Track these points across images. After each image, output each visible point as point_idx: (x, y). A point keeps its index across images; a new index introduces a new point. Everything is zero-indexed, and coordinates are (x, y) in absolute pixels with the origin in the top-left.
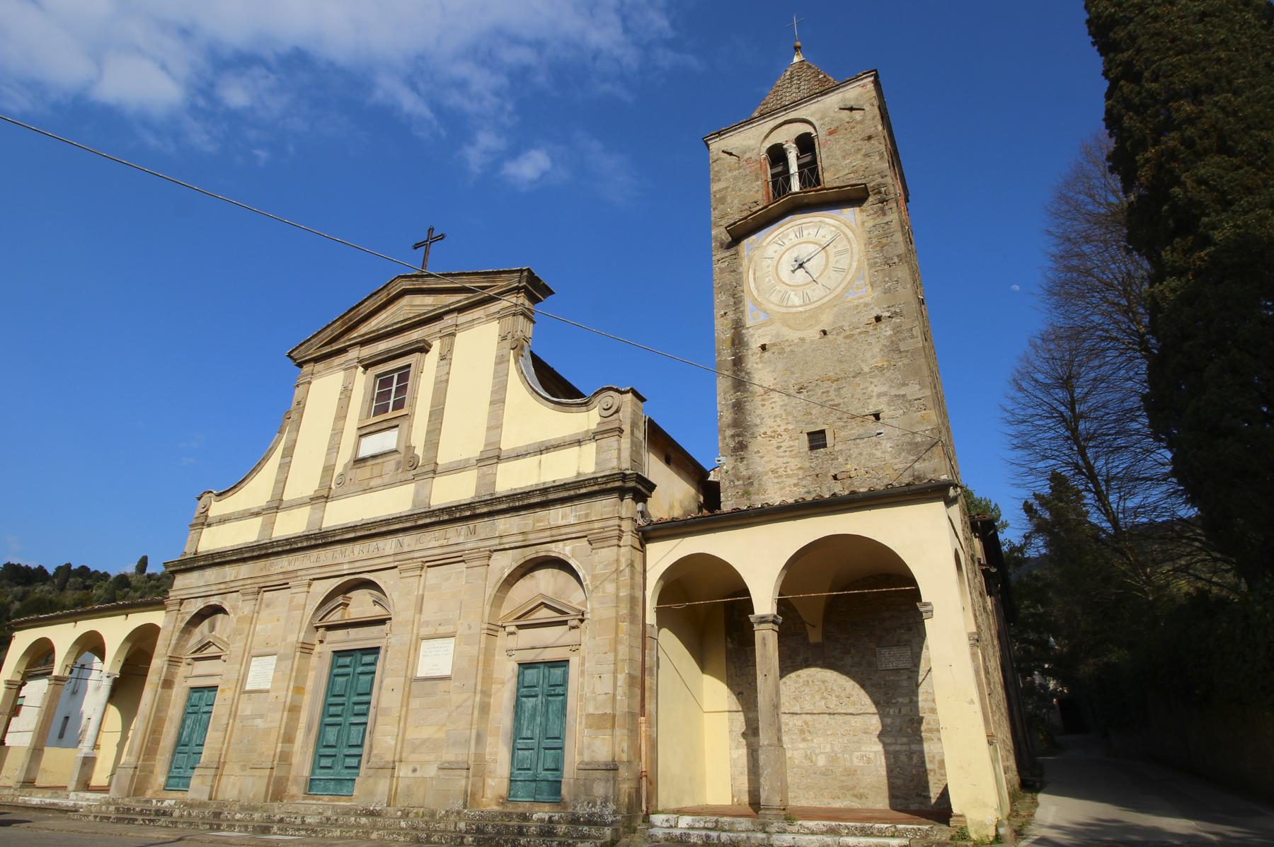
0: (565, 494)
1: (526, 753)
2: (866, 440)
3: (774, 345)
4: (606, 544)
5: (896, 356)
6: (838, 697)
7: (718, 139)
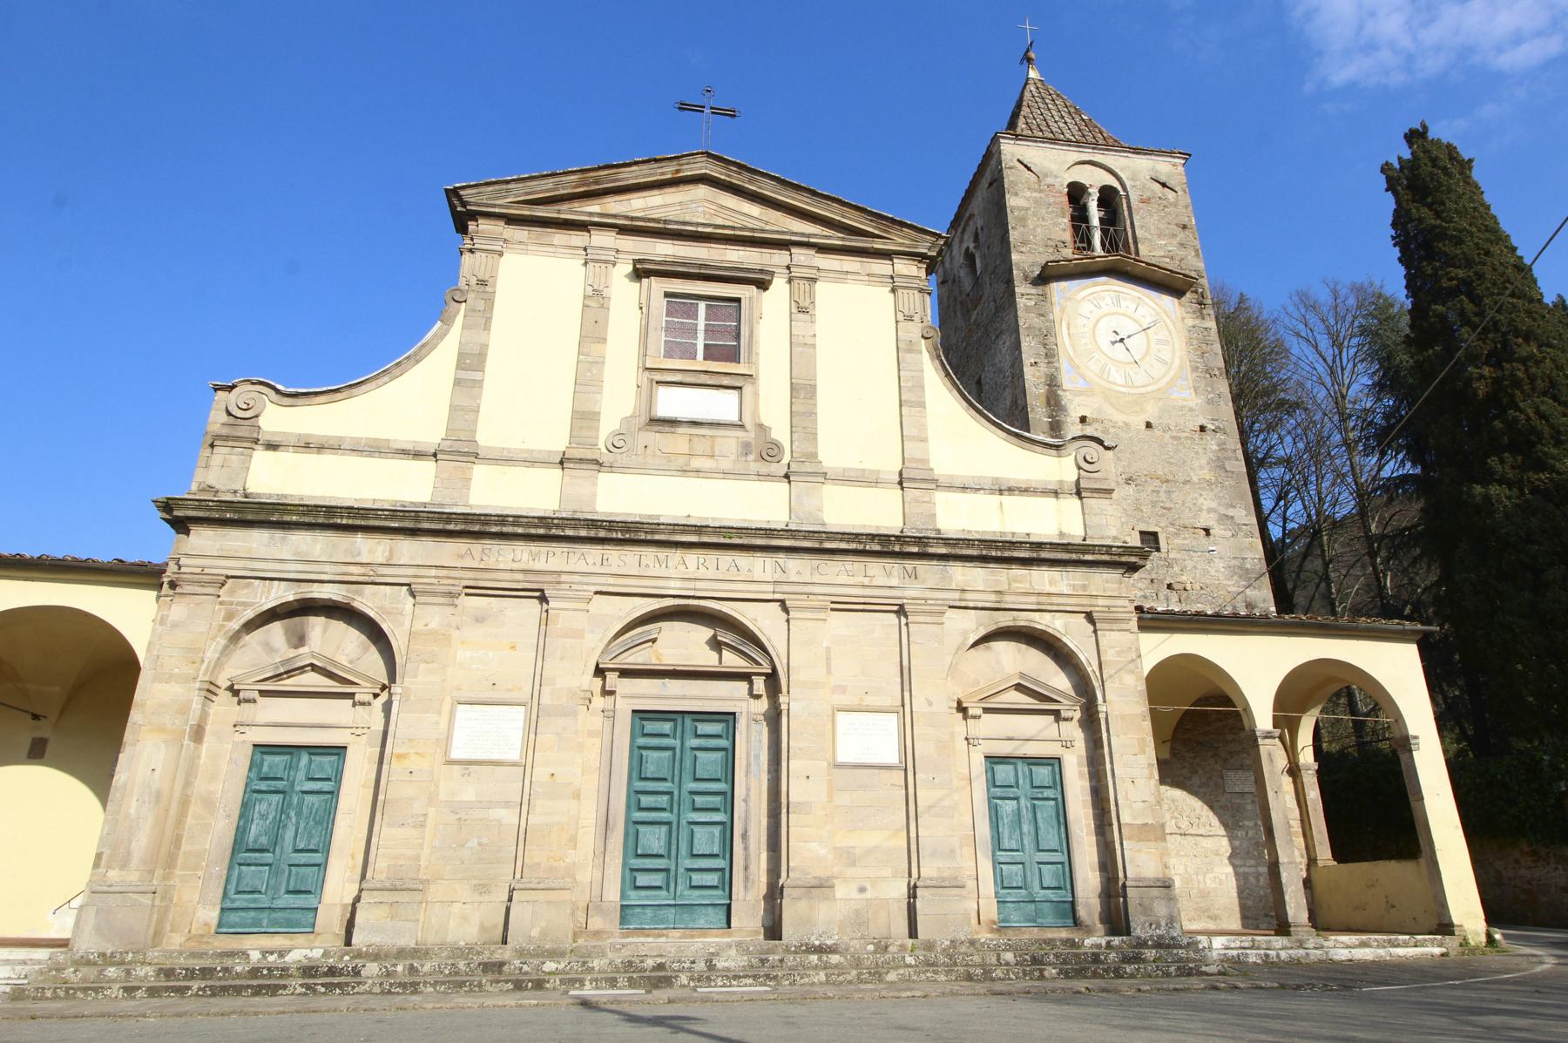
0: (1065, 556)
1: (1014, 867)
2: (1199, 554)
3: (1096, 420)
4: (1115, 626)
5: (1223, 475)
6: (1188, 817)
7: (1012, 142)
